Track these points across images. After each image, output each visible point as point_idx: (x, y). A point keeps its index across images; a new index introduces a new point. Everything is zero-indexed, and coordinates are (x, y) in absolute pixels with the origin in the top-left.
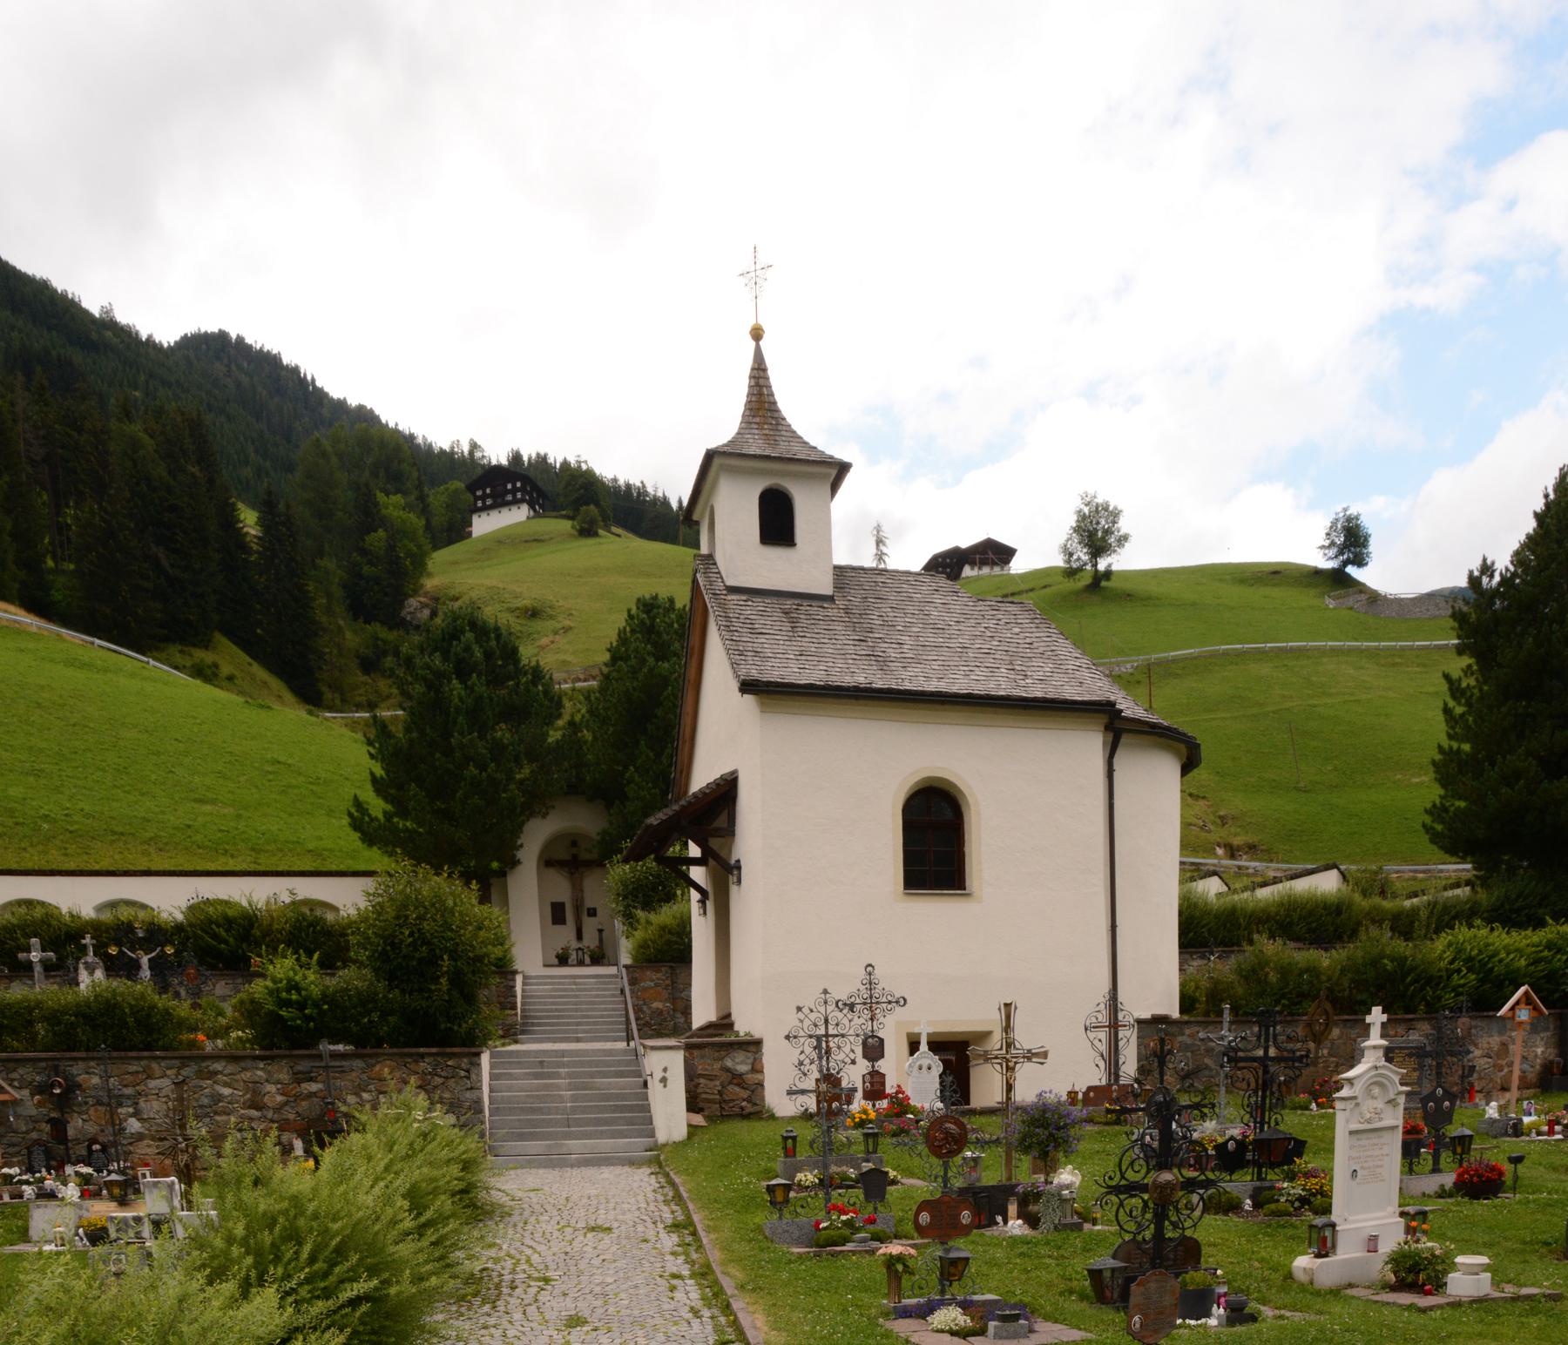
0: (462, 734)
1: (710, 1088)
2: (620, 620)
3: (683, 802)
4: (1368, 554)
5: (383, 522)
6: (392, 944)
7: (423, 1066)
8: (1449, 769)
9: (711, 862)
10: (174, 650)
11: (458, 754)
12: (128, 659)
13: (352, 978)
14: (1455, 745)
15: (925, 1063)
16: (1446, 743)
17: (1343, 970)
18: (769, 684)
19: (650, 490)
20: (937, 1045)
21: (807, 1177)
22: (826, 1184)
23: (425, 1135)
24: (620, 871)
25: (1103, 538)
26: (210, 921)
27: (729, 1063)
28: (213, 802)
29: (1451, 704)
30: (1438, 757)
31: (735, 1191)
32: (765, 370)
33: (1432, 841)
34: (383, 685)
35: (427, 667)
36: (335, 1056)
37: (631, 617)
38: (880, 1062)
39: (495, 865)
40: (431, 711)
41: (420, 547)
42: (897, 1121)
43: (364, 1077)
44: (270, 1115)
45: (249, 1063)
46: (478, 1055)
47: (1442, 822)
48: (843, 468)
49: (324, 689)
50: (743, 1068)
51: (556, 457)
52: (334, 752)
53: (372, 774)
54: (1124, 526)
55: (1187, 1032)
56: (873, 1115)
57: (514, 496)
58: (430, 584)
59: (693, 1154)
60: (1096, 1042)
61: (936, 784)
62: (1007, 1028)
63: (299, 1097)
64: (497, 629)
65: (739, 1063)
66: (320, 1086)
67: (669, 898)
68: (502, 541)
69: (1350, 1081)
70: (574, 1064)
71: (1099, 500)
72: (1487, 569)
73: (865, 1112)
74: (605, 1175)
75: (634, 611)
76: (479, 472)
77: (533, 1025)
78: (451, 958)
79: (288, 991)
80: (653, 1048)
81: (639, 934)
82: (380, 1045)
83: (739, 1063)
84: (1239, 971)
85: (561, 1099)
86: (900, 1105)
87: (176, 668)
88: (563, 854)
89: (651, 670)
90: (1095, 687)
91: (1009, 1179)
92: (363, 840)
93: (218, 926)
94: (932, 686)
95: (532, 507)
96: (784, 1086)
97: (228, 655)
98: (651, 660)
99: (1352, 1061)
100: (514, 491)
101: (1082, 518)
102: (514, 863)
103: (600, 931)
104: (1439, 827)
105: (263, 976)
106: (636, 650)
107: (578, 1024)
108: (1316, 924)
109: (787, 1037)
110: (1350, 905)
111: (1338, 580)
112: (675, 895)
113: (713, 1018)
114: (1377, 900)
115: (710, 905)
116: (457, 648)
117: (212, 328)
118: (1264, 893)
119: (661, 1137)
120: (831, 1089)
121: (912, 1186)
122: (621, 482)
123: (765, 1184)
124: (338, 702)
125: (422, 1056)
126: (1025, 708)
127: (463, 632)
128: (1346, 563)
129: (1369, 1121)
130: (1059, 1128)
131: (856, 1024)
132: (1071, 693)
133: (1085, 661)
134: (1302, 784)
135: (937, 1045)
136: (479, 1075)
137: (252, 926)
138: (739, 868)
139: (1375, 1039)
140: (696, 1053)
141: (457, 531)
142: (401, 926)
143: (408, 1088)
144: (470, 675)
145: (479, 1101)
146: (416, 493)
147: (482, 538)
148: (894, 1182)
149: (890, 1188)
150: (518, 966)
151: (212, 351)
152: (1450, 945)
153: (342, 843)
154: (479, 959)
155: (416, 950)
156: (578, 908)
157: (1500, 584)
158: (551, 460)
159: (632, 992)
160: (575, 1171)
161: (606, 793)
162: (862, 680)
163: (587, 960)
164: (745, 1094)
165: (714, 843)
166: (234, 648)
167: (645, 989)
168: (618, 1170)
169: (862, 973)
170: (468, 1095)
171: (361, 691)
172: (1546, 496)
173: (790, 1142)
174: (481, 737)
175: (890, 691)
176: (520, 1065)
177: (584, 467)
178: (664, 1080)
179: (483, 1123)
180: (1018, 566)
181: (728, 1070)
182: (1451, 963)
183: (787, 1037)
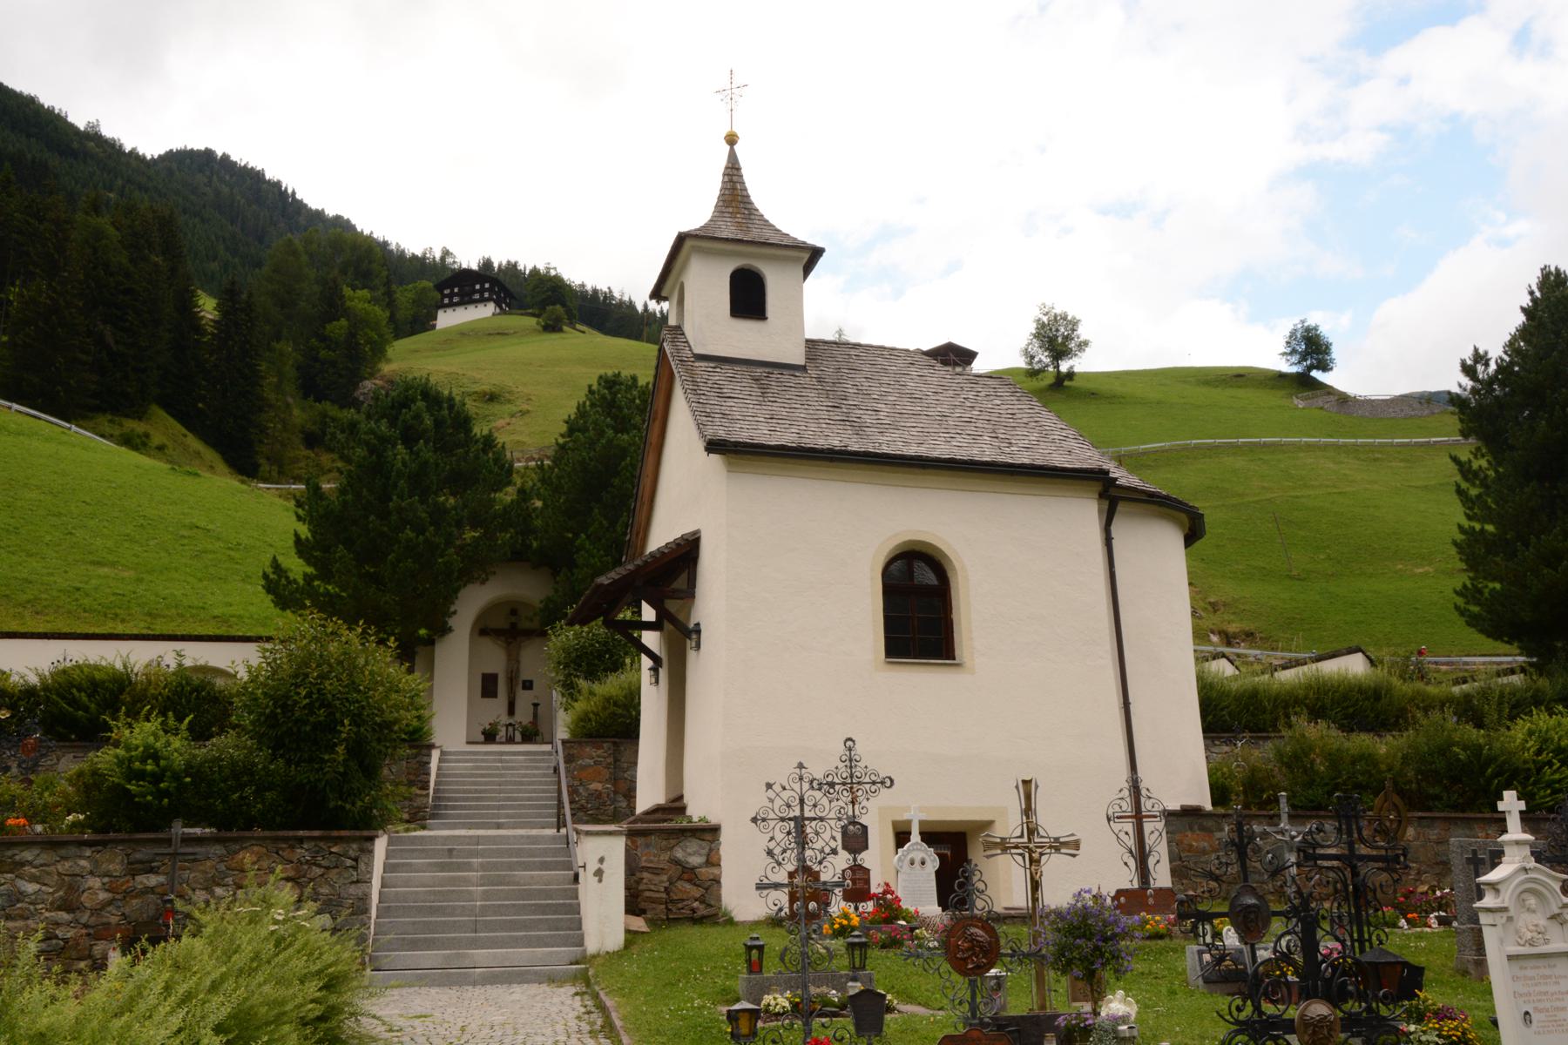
0: (401, 497)
1: (655, 885)
2: (582, 396)
3: (638, 562)
4: (1332, 360)
5: (347, 313)
6: (284, 706)
7: (301, 853)
8: (1473, 550)
9: (668, 626)
10: (103, 421)
11: (394, 517)
12: (49, 424)
13: (226, 745)
14: (1478, 526)
15: (918, 856)
16: (1466, 523)
17: (1405, 757)
18: (737, 444)
19: (617, 295)
20: (932, 836)
21: (779, 1000)
22: (803, 1010)
23: (279, 942)
24: (566, 636)
25: (1063, 344)
26: (71, 685)
27: (679, 854)
28: (113, 565)
29: (1464, 485)
30: (1460, 537)
31: (683, 1018)
32: (739, 169)
33: (1468, 624)
34: (326, 459)
35: (372, 432)
36: (188, 840)
37: (591, 392)
38: (863, 855)
39: (423, 632)
40: (372, 476)
41: (381, 336)
42: (887, 928)
43: (222, 867)
44: (85, 918)
45: (73, 850)
46: (371, 839)
47: (1478, 604)
48: (816, 253)
49: (262, 461)
50: (696, 860)
51: (526, 263)
52: (264, 519)
53: (296, 535)
54: (1083, 332)
56: (856, 921)
58: (385, 369)
59: (630, 968)
60: (1122, 835)
61: (917, 548)
62: (1028, 810)
63: (129, 894)
64: (451, 399)
65: (692, 854)
66: (162, 879)
67: (616, 667)
68: (465, 333)
69: (1494, 886)
70: (491, 853)
71: (1058, 311)
72: (1480, 358)
73: (846, 916)
74: (516, 997)
75: (595, 387)
76: (449, 274)
77: (446, 807)
78: (353, 722)
79: (143, 761)
80: (588, 833)
81: (580, 706)
82: (249, 828)
83: (692, 854)
84: (1280, 754)
85: (470, 896)
86: (889, 909)
87: (102, 436)
88: (501, 622)
89: (610, 441)
90: (1084, 456)
91: (1043, 1007)
92: (276, 604)
93: (80, 689)
94: (912, 450)
95: (498, 304)
96: (747, 886)
97: (162, 426)
98: (610, 433)
99: (1496, 858)
100: (482, 291)
101: (1041, 326)
102: (445, 630)
103: (536, 705)
104: (1475, 609)
105: (116, 744)
106: (595, 423)
107: (499, 808)
108: (1357, 708)
109: (754, 820)
110: (1389, 689)
111: (1303, 383)
112: (623, 664)
113: (661, 799)
114: (1420, 685)
115: (663, 673)
116: (406, 415)
117: (198, 145)
118: (1287, 676)
119: (592, 946)
120: (807, 891)
121: (914, 1015)
122: (589, 288)
123: (725, 1009)
124: (274, 474)
125: (301, 840)
126: (1012, 474)
127: (414, 401)
129: (1531, 943)
130: (1105, 939)
131: (831, 808)
132: (1059, 460)
133: (1071, 432)
134: (1295, 572)
135: (932, 836)
136: (370, 864)
137: (122, 690)
138: (698, 632)
139: (1515, 831)
140: (640, 841)
141: (421, 322)
142: (297, 686)
143: (272, 878)
144: (417, 441)
145: (365, 899)
146: (382, 290)
147: (446, 331)
148: (890, 1009)
149: (888, 1017)
150: (436, 740)
151: (198, 169)
152: (1531, 733)
153: (253, 609)
154: (388, 725)
155: (312, 713)
156: (512, 680)
157: (1497, 372)
158: (521, 267)
159: (567, 771)
160: (478, 990)
161: (553, 560)
162: (836, 443)
163: (518, 737)
164: (697, 892)
165: (672, 605)
166: (172, 421)
167: (583, 768)
168: (534, 989)
169: (841, 749)
170: (352, 890)
171: (302, 464)
172: (1531, 293)
173: (755, 952)
174: (422, 502)
175: (867, 454)
176: (425, 853)
177: (553, 273)
178: (599, 873)
179: (365, 924)
180: (978, 366)
181: (677, 862)
182: (1539, 752)
183: (754, 820)
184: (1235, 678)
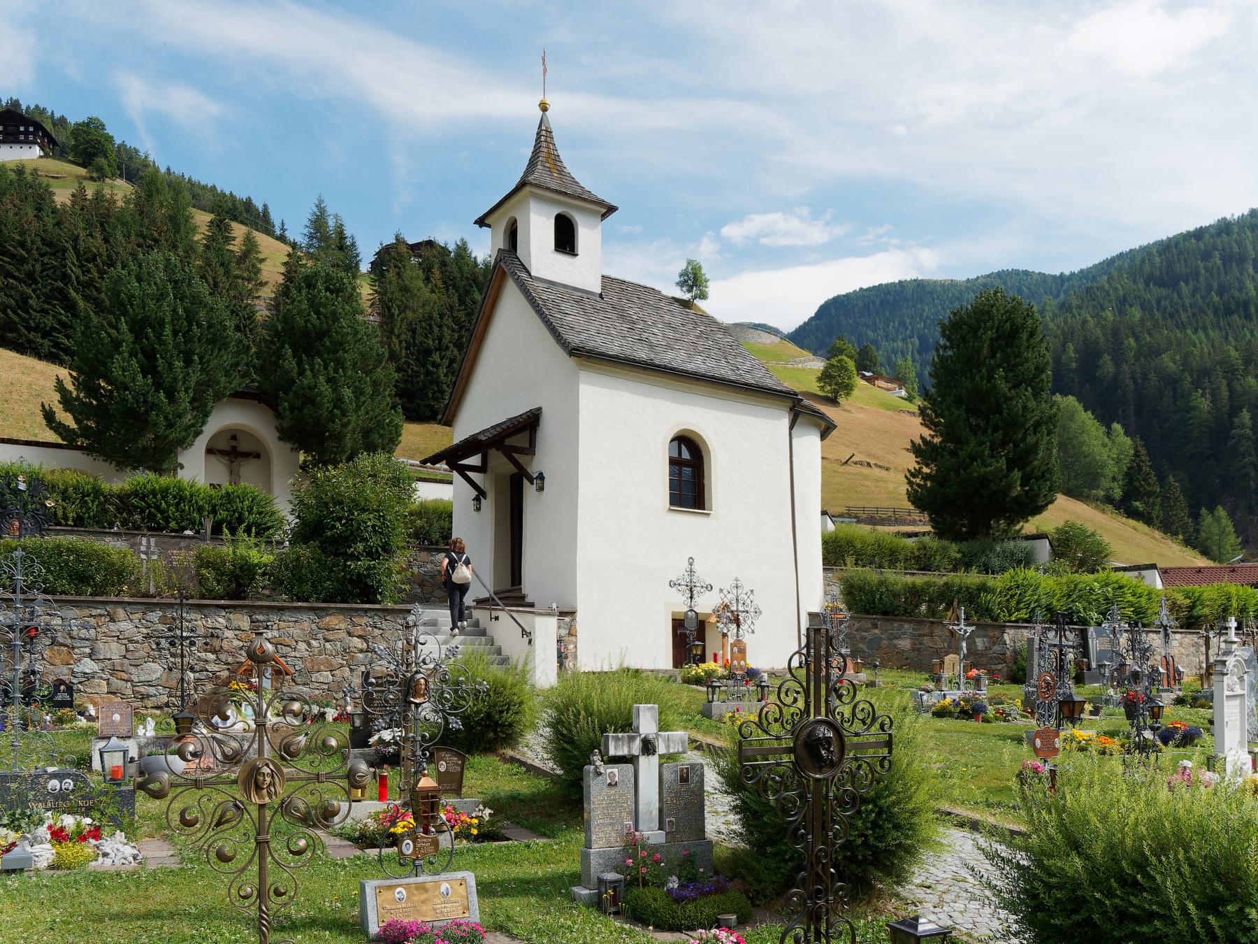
48: (611, 209)
57: (27, 137)
61: (693, 437)
88: (225, 446)
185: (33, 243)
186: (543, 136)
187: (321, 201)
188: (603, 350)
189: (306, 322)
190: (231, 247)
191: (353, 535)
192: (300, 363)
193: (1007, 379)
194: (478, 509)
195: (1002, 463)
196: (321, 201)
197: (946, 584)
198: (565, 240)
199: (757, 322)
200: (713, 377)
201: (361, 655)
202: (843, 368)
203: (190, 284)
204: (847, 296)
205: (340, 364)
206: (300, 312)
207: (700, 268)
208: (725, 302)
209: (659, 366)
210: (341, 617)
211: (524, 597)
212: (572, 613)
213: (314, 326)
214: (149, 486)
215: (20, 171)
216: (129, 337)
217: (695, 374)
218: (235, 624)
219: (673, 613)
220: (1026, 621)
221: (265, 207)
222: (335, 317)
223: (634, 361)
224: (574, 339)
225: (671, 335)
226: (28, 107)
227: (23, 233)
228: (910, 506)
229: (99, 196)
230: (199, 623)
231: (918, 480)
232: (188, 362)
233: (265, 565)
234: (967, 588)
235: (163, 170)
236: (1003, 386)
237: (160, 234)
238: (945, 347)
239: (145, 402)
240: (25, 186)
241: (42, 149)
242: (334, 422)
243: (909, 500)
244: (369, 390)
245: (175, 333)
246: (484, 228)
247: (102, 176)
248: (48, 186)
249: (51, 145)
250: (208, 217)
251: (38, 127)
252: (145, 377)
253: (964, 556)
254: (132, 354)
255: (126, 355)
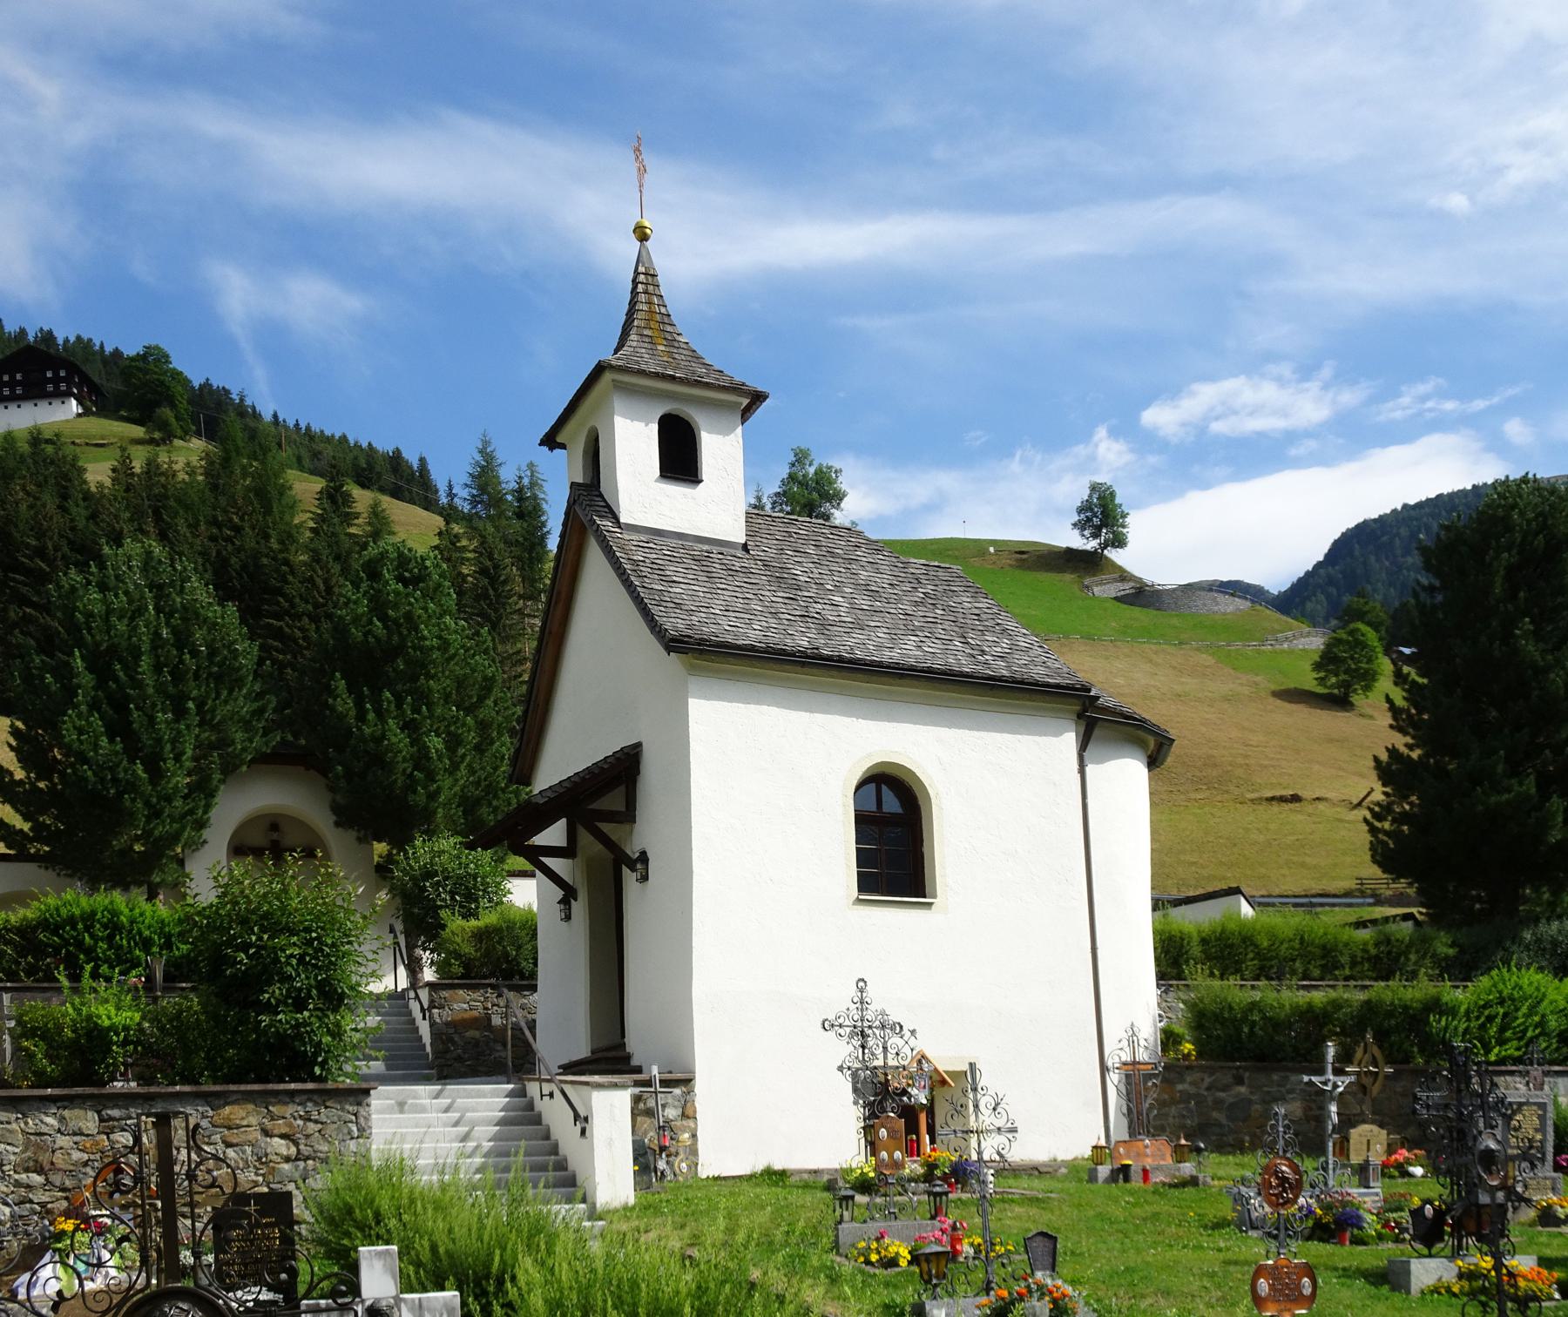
48: (758, 398)
55: (1189, 1079)
57: (57, 387)
61: (888, 771)
88: (258, 838)
100: (56, 380)
128: (1105, 546)
169: (852, 991)
184: (1255, 921)
185: (56, 549)
186: (644, 280)
187: (486, 443)
188: (729, 639)
189: (365, 635)
190: (353, 530)
191: (267, 969)
192: (359, 704)
193: (1537, 635)
194: (568, 918)
195: (1530, 785)
196: (486, 443)
197: (1368, 1002)
198: (680, 459)
199: (1225, 577)
200: (930, 670)
201: (286, 1166)
202: (1359, 644)
203: (182, 591)
204: (1382, 520)
205: (423, 697)
206: (356, 620)
207: (1113, 494)
208: (1168, 544)
209: (829, 658)
210: (251, 1107)
211: (628, 1057)
212: (687, 1082)
213: (378, 640)
214: (64, 912)
215: (36, 438)
216: (87, 679)
217: (897, 666)
218: (73, 1125)
219: (969, 1077)
220: (1518, 1061)
221: (422, 460)
222: (411, 621)
223: (783, 652)
224: (675, 623)
225: (864, 602)
226: (67, 340)
227: (41, 534)
228: (1376, 871)
229: (152, 466)
230: (14, 1126)
231: (1387, 825)
232: (180, 713)
233: (126, 1028)
234: (1406, 1008)
235: (267, 416)
236: (1530, 648)
237: (242, 519)
238: (1431, 589)
239: (115, 780)
240: (48, 461)
241: (80, 402)
242: (415, 792)
243: (1374, 861)
244: (472, 737)
245: (157, 668)
246: (557, 451)
247: (168, 437)
248: (75, 458)
249: (98, 401)
250: (318, 484)
251: (73, 369)
252: (112, 741)
253: (1462, 951)
254: (94, 706)
255: (83, 708)
